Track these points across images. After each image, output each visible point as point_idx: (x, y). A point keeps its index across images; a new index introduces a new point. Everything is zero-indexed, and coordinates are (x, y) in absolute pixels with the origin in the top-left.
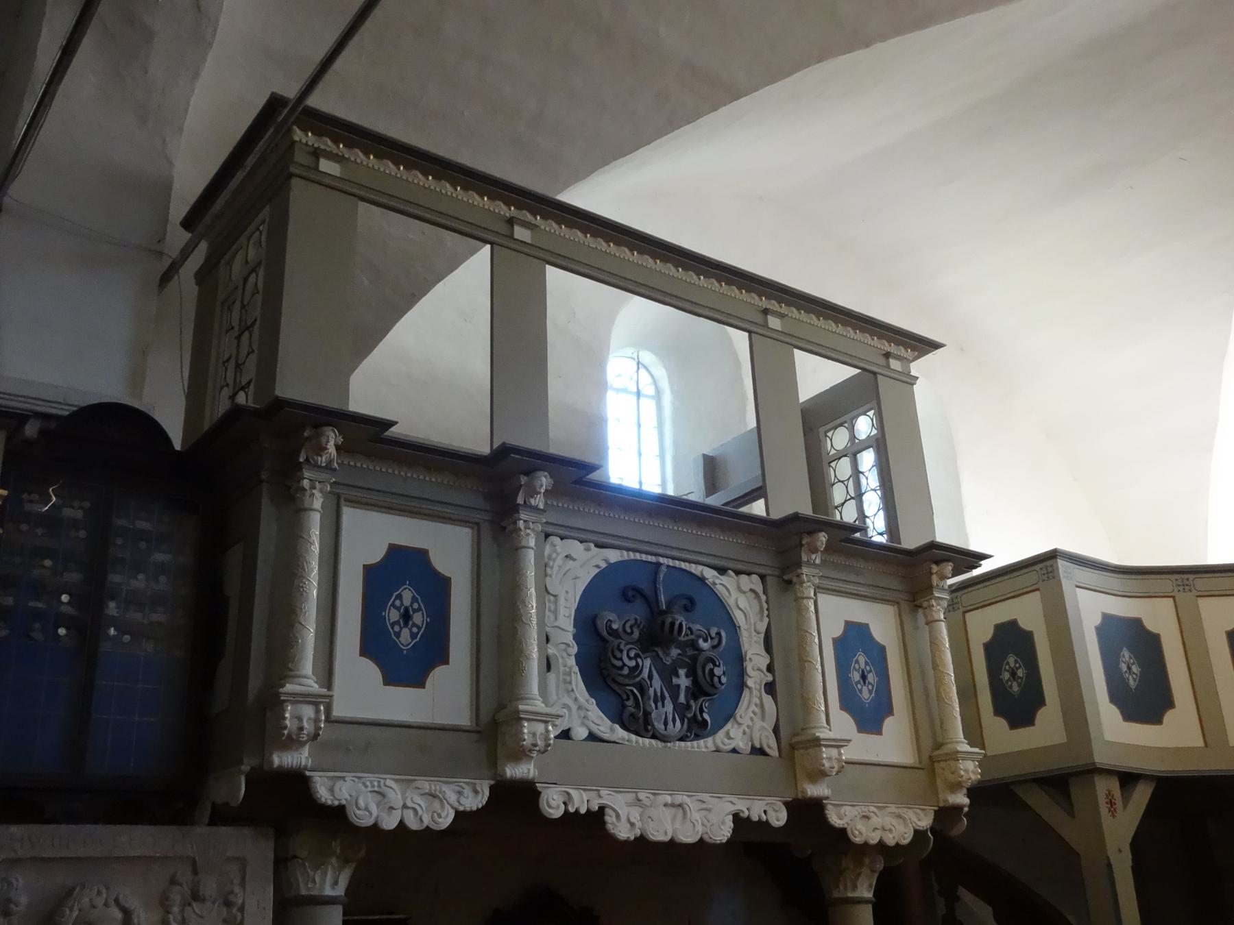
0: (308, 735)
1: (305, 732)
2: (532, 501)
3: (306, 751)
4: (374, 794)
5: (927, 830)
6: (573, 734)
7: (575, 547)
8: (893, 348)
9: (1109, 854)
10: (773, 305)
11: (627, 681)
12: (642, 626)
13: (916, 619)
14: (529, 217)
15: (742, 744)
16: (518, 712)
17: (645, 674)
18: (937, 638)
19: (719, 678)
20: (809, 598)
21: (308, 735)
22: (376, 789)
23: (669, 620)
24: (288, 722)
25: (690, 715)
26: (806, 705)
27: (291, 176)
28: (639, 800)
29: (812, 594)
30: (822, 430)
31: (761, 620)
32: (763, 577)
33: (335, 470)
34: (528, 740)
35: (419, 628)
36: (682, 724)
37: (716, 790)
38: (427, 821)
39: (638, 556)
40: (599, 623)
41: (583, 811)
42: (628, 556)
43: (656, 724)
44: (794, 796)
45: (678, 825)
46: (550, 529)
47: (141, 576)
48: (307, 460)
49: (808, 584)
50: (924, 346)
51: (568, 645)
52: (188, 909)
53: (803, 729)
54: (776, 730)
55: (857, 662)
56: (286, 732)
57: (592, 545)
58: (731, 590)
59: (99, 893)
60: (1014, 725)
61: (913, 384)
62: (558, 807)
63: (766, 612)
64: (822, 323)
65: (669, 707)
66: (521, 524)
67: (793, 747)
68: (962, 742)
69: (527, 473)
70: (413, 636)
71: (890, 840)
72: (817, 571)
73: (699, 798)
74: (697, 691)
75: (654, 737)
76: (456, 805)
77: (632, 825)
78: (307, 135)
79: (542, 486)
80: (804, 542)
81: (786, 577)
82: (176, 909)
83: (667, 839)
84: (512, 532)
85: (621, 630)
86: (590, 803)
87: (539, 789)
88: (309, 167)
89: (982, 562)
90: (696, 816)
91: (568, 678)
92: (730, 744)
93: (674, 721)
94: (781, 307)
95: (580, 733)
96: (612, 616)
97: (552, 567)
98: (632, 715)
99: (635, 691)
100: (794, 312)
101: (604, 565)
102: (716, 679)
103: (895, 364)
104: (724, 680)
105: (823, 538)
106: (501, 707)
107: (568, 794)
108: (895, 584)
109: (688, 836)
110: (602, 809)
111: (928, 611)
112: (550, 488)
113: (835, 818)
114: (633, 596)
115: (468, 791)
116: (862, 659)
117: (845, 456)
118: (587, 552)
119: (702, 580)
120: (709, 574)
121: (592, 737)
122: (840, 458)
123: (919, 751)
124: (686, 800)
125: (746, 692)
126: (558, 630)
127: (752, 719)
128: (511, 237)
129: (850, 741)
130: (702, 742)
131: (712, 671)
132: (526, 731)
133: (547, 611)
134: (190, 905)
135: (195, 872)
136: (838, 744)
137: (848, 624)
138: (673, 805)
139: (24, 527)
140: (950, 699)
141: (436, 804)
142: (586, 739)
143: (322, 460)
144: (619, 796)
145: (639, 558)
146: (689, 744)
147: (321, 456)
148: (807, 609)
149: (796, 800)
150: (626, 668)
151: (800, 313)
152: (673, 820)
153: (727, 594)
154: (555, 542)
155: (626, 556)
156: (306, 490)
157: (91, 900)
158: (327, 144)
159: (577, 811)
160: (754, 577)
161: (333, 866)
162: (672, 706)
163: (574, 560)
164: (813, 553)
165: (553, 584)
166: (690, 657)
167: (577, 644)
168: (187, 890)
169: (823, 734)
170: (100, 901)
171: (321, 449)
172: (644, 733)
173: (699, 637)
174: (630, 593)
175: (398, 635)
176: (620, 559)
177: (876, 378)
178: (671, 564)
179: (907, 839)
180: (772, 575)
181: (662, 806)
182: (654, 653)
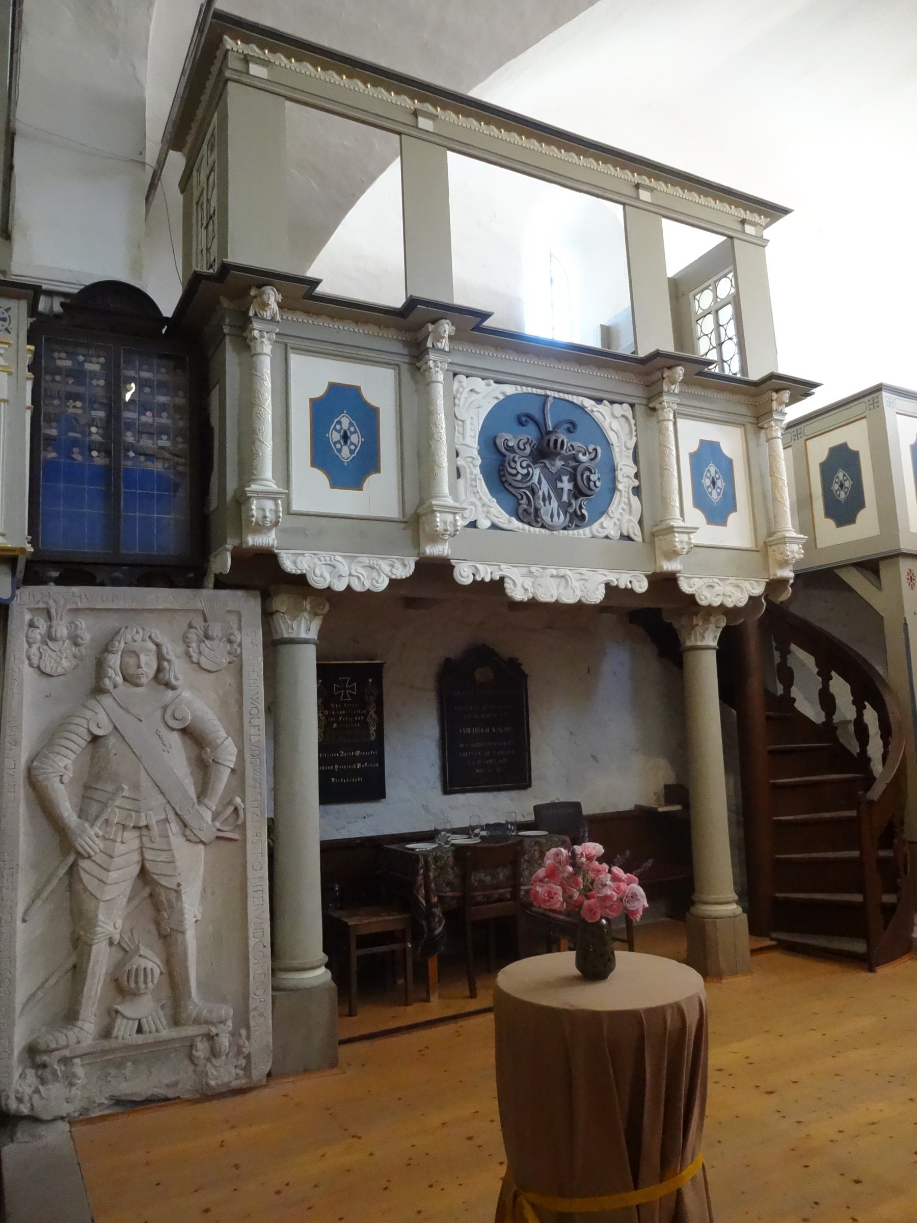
0: (271, 522)
1: (268, 519)
2: (439, 345)
3: (273, 534)
4: (328, 567)
5: (760, 597)
6: (478, 524)
7: (478, 383)
8: (748, 216)
9: (906, 615)
10: (645, 180)
11: (520, 485)
12: (533, 444)
13: (758, 438)
14: (429, 107)
15: (614, 533)
16: (431, 506)
17: (535, 480)
18: (774, 451)
19: (595, 482)
20: (669, 420)
21: (271, 522)
22: (328, 562)
23: (553, 438)
24: (254, 513)
25: (571, 510)
26: (662, 502)
27: (227, 80)
28: (531, 573)
29: (671, 417)
30: (691, 295)
31: (631, 439)
32: (632, 406)
33: (278, 322)
34: (440, 527)
35: (356, 447)
36: (565, 517)
37: (592, 566)
38: (368, 585)
39: (530, 390)
40: (498, 441)
41: (487, 579)
42: (522, 389)
43: (544, 517)
44: (653, 571)
45: (561, 590)
46: (458, 369)
47: (149, 413)
48: (256, 314)
49: (669, 409)
50: (775, 211)
51: (473, 458)
52: (203, 645)
53: (661, 521)
54: (640, 522)
55: (709, 471)
56: (254, 519)
57: (492, 382)
58: (606, 417)
59: (137, 632)
60: (840, 523)
61: (764, 247)
62: (468, 576)
63: (634, 433)
64: (686, 195)
65: (555, 504)
66: (431, 363)
67: (653, 535)
68: (790, 531)
69: (434, 322)
70: (352, 452)
71: (730, 604)
72: (676, 399)
73: (579, 571)
74: (578, 492)
75: (543, 527)
76: (390, 574)
77: (526, 590)
78: (237, 44)
79: (445, 331)
80: (664, 376)
81: (651, 405)
82: (194, 645)
83: (553, 600)
84: (425, 371)
85: (515, 446)
86: (493, 574)
87: (454, 564)
88: (241, 72)
89: (814, 390)
90: (576, 584)
91: (474, 483)
92: (603, 532)
93: (559, 515)
94: (651, 181)
95: (485, 523)
96: (508, 436)
97: (459, 399)
98: (525, 511)
99: (528, 492)
100: (661, 186)
101: (502, 397)
102: (592, 484)
103: (749, 229)
104: (598, 484)
105: (680, 371)
106: (422, 502)
107: (476, 568)
108: (743, 410)
109: (569, 598)
110: (502, 579)
111: (768, 430)
112: (453, 334)
113: (686, 586)
114: (526, 421)
115: (398, 565)
116: (713, 469)
117: (710, 313)
118: (487, 387)
119: (582, 408)
120: (588, 404)
121: (494, 526)
122: (705, 316)
123: (756, 538)
124: (568, 572)
125: (617, 494)
126: (465, 447)
127: (621, 514)
128: (416, 127)
129: (697, 528)
130: (581, 531)
131: (588, 477)
132: (438, 520)
133: (456, 433)
134: (204, 642)
135: (205, 620)
136: (689, 531)
137: (702, 442)
138: (558, 576)
139: (58, 378)
140: (783, 498)
141: (375, 574)
142: (489, 528)
143: (268, 314)
144: (515, 569)
145: (525, 391)
146: (571, 532)
147: (266, 311)
148: (667, 429)
149: (654, 574)
150: (519, 475)
151: (667, 187)
152: (558, 586)
153: (603, 419)
154: (461, 380)
155: (520, 389)
156: (256, 338)
157: (132, 637)
158: (253, 50)
159: (483, 580)
160: (626, 406)
161: (305, 618)
162: (557, 504)
163: (477, 393)
164: (673, 384)
165: (460, 412)
166: (571, 467)
167: (481, 458)
168: (201, 633)
169: (677, 523)
170: (138, 637)
171: (265, 305)
172: (535, 524)
173: (579, 452)
174: (524, 419)
175: (340, 451)
176: (516, 392)
177: (733, 244)
178: (557, 396)
179: (743, 602)
180: (641, 404)
181: (549, 578)
182: (542, 465)
